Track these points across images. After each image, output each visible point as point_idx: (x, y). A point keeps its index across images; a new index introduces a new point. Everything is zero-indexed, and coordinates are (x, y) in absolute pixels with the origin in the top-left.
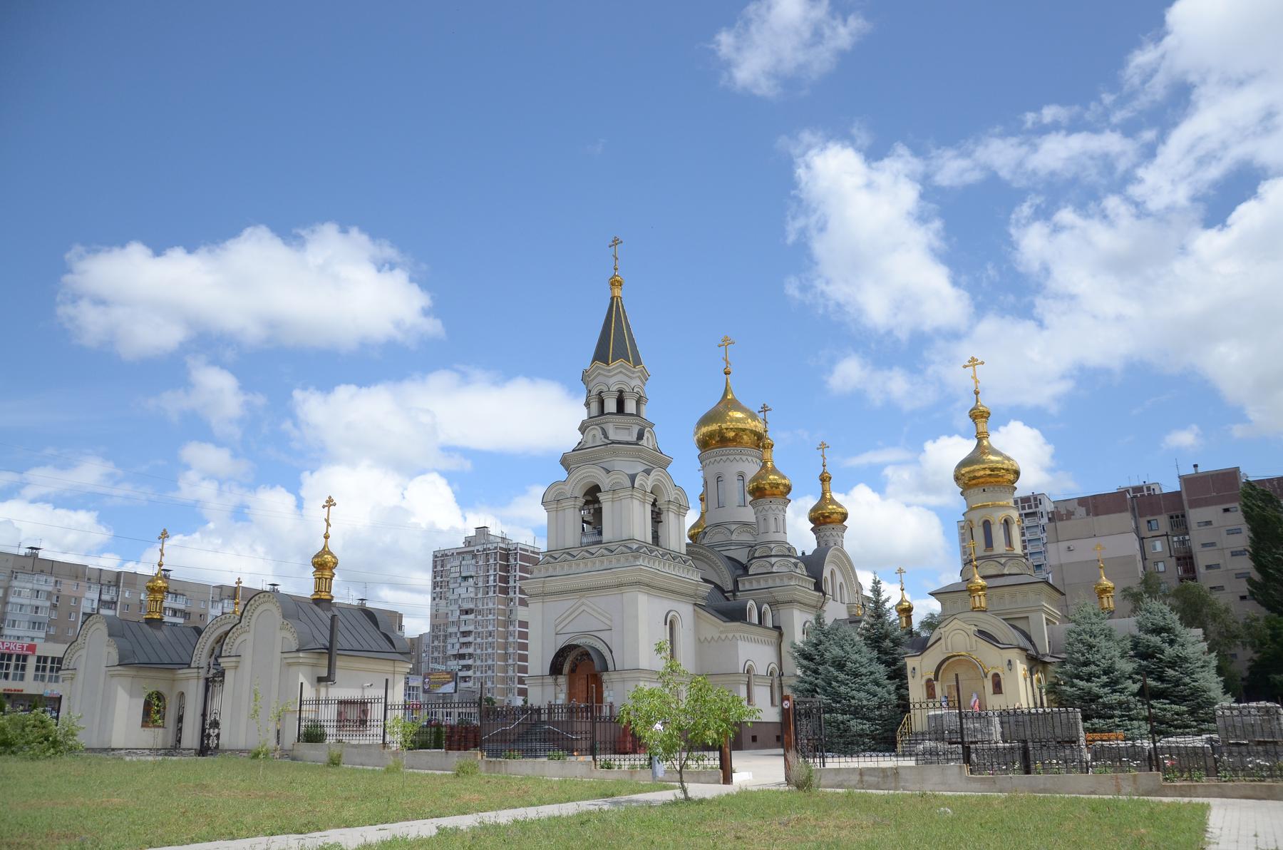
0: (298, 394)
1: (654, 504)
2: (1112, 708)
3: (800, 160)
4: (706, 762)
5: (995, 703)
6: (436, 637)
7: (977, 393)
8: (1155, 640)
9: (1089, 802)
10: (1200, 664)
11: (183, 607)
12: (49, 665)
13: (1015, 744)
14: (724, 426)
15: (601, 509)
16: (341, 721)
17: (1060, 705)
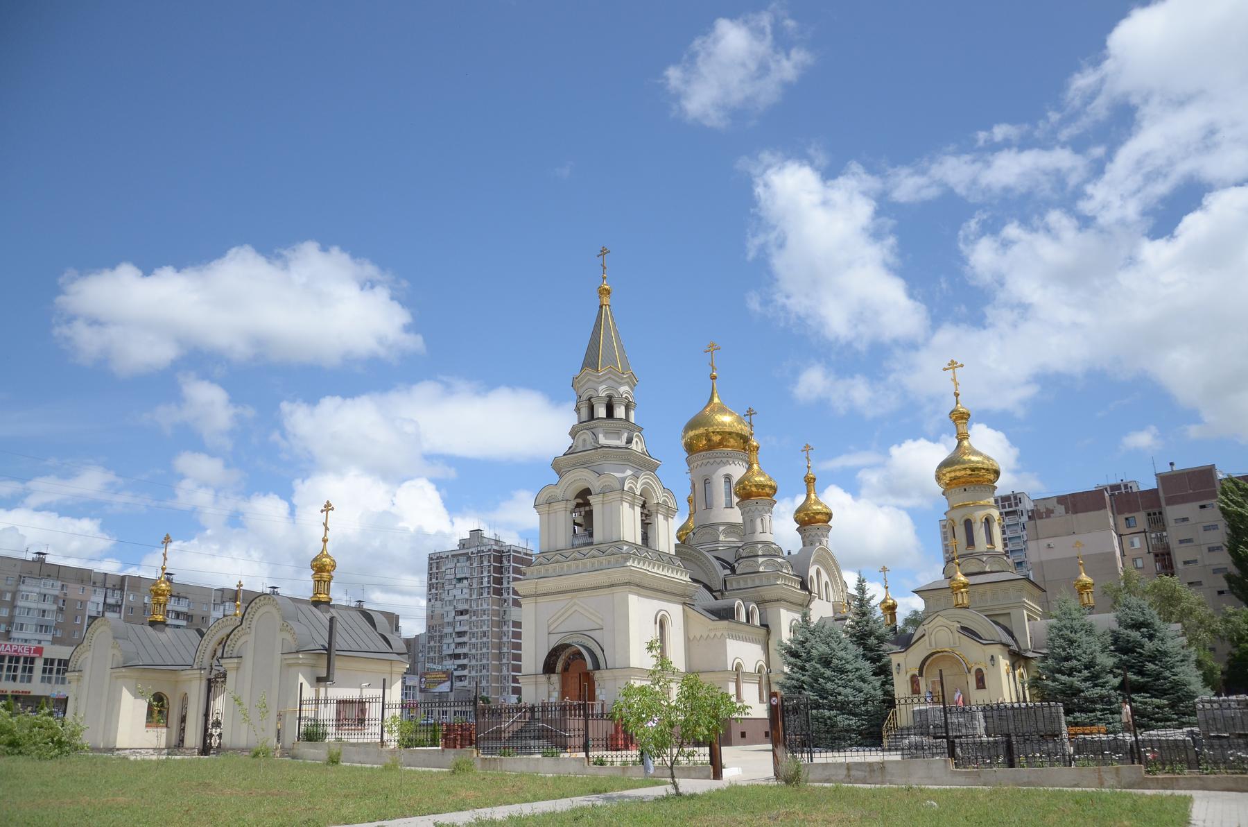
0: (285, 406)
1: (643, 506)
2: (1093, 701)
3: (757, 180)
4: (696, 758)
5: (979, 698)
6: (431, 638)
7: (957, 395)
8: (1135, 635)
9: (1073, 794)
10: (1180, 658)
11: (185, 610)
12: (55, 667)
13: (999, 738)
14: (711, 429)
15: (591, 511)
16: (340, 722)
17: (1043, 699)
